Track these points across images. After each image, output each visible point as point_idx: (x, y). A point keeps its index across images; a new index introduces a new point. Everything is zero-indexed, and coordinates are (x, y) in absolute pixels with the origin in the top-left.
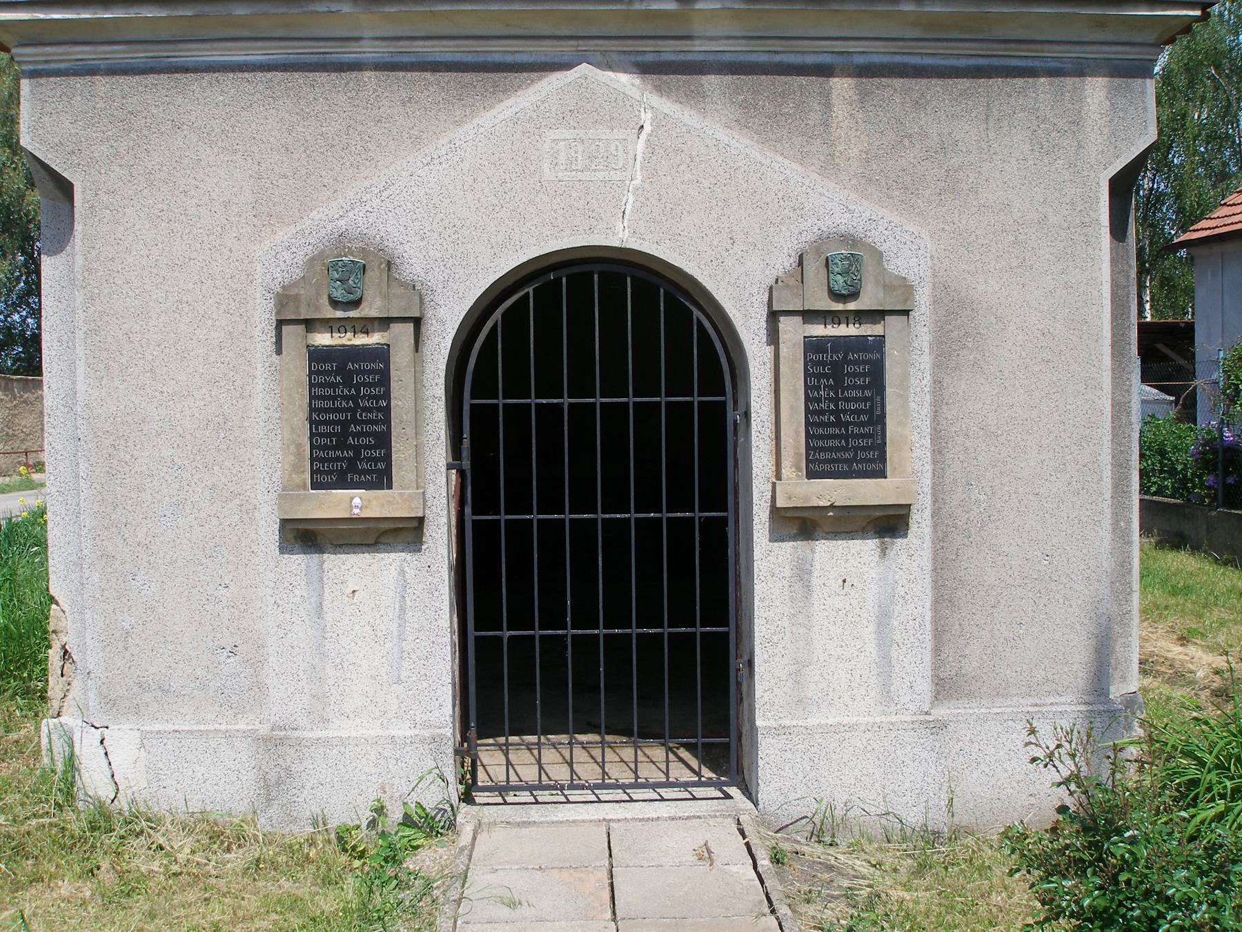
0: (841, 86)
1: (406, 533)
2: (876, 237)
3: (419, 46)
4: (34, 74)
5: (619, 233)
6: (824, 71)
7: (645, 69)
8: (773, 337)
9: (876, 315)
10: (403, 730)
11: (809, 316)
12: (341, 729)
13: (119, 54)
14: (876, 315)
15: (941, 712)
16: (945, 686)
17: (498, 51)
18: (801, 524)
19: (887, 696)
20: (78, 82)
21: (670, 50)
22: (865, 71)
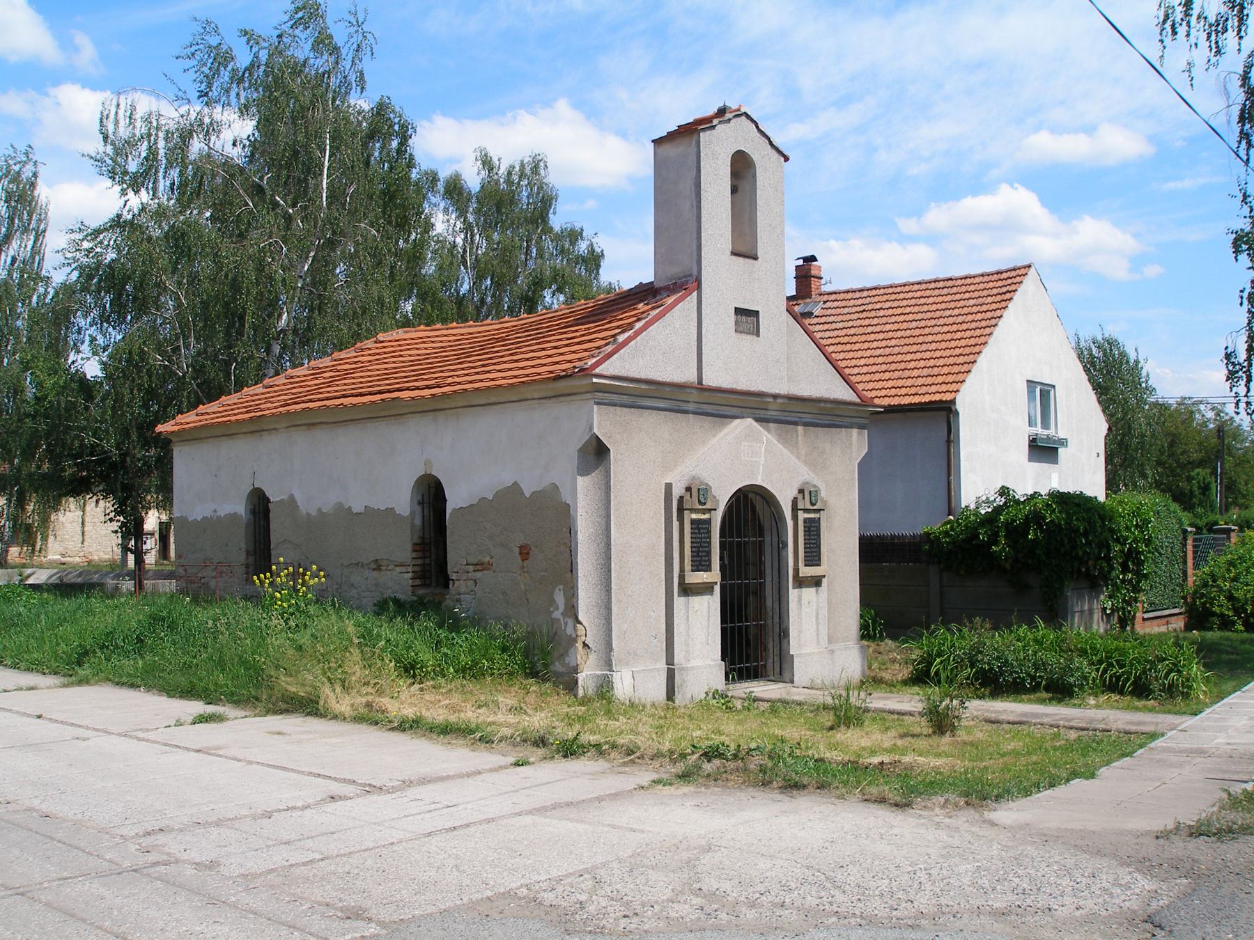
0: (800, 428)
1: (706, 589)
2: (755, 157)
3: (705, 407)
4: (598, 404)
5: (759, 482)
6: (796, 423)
7: (757, 420)
8: (795, 518)
9: (818, 511)
10: (709, 662)
11: (806, 511)
12: (693, 663)
13: (625, 399)
14: (818, 511)
15: (832, 647)
16: (831, 640)
17: (723, 410)
18: (801, 582)
19: (818, 643)
20: (612, 409)
21: (762, 414)
22: (806, 424)
